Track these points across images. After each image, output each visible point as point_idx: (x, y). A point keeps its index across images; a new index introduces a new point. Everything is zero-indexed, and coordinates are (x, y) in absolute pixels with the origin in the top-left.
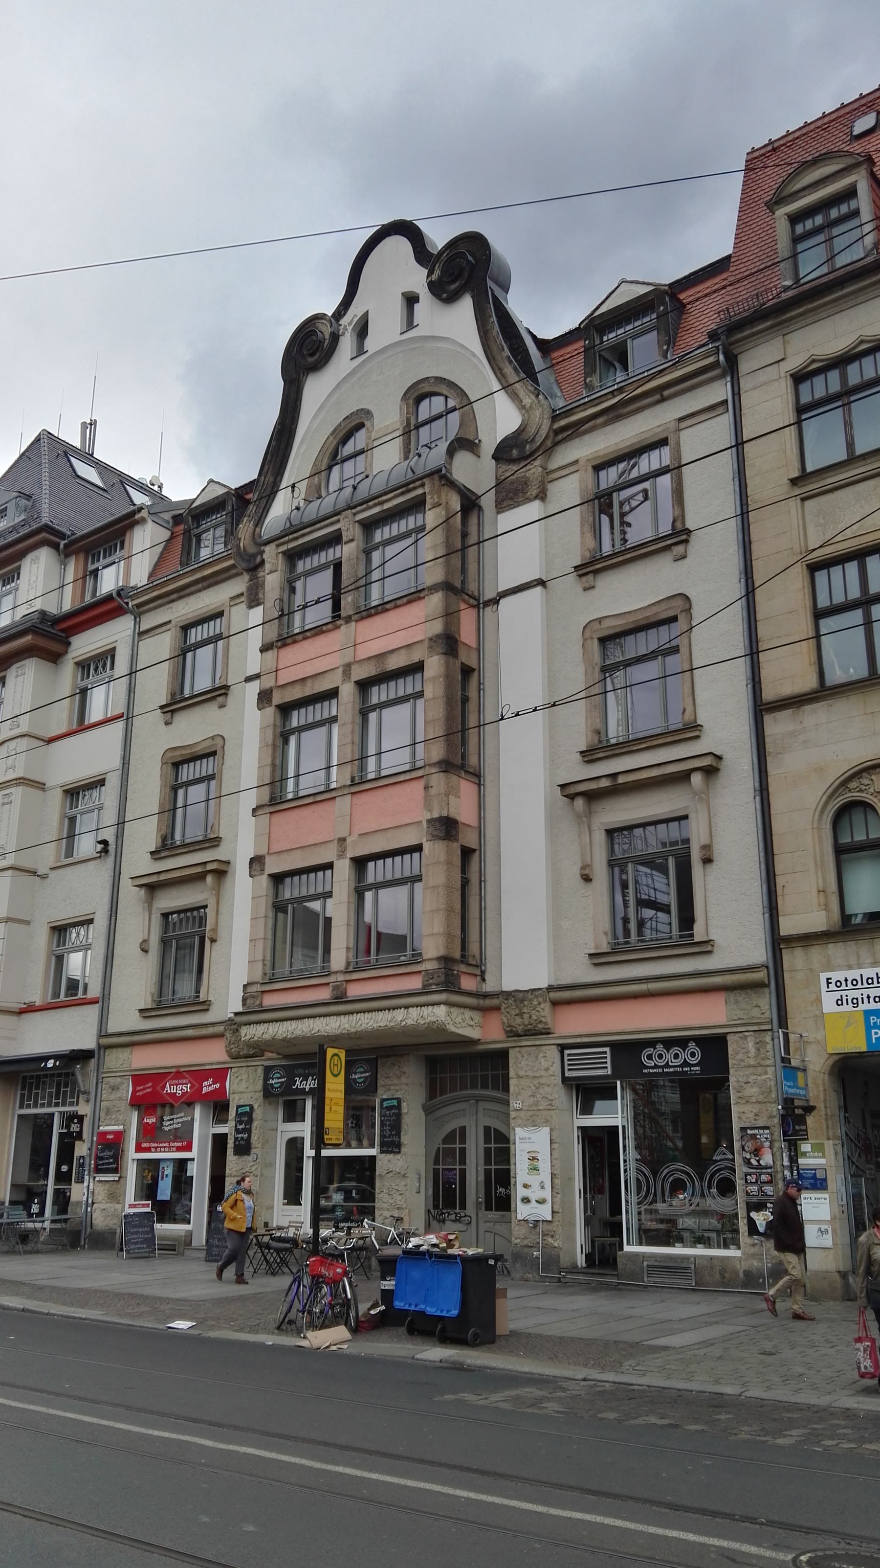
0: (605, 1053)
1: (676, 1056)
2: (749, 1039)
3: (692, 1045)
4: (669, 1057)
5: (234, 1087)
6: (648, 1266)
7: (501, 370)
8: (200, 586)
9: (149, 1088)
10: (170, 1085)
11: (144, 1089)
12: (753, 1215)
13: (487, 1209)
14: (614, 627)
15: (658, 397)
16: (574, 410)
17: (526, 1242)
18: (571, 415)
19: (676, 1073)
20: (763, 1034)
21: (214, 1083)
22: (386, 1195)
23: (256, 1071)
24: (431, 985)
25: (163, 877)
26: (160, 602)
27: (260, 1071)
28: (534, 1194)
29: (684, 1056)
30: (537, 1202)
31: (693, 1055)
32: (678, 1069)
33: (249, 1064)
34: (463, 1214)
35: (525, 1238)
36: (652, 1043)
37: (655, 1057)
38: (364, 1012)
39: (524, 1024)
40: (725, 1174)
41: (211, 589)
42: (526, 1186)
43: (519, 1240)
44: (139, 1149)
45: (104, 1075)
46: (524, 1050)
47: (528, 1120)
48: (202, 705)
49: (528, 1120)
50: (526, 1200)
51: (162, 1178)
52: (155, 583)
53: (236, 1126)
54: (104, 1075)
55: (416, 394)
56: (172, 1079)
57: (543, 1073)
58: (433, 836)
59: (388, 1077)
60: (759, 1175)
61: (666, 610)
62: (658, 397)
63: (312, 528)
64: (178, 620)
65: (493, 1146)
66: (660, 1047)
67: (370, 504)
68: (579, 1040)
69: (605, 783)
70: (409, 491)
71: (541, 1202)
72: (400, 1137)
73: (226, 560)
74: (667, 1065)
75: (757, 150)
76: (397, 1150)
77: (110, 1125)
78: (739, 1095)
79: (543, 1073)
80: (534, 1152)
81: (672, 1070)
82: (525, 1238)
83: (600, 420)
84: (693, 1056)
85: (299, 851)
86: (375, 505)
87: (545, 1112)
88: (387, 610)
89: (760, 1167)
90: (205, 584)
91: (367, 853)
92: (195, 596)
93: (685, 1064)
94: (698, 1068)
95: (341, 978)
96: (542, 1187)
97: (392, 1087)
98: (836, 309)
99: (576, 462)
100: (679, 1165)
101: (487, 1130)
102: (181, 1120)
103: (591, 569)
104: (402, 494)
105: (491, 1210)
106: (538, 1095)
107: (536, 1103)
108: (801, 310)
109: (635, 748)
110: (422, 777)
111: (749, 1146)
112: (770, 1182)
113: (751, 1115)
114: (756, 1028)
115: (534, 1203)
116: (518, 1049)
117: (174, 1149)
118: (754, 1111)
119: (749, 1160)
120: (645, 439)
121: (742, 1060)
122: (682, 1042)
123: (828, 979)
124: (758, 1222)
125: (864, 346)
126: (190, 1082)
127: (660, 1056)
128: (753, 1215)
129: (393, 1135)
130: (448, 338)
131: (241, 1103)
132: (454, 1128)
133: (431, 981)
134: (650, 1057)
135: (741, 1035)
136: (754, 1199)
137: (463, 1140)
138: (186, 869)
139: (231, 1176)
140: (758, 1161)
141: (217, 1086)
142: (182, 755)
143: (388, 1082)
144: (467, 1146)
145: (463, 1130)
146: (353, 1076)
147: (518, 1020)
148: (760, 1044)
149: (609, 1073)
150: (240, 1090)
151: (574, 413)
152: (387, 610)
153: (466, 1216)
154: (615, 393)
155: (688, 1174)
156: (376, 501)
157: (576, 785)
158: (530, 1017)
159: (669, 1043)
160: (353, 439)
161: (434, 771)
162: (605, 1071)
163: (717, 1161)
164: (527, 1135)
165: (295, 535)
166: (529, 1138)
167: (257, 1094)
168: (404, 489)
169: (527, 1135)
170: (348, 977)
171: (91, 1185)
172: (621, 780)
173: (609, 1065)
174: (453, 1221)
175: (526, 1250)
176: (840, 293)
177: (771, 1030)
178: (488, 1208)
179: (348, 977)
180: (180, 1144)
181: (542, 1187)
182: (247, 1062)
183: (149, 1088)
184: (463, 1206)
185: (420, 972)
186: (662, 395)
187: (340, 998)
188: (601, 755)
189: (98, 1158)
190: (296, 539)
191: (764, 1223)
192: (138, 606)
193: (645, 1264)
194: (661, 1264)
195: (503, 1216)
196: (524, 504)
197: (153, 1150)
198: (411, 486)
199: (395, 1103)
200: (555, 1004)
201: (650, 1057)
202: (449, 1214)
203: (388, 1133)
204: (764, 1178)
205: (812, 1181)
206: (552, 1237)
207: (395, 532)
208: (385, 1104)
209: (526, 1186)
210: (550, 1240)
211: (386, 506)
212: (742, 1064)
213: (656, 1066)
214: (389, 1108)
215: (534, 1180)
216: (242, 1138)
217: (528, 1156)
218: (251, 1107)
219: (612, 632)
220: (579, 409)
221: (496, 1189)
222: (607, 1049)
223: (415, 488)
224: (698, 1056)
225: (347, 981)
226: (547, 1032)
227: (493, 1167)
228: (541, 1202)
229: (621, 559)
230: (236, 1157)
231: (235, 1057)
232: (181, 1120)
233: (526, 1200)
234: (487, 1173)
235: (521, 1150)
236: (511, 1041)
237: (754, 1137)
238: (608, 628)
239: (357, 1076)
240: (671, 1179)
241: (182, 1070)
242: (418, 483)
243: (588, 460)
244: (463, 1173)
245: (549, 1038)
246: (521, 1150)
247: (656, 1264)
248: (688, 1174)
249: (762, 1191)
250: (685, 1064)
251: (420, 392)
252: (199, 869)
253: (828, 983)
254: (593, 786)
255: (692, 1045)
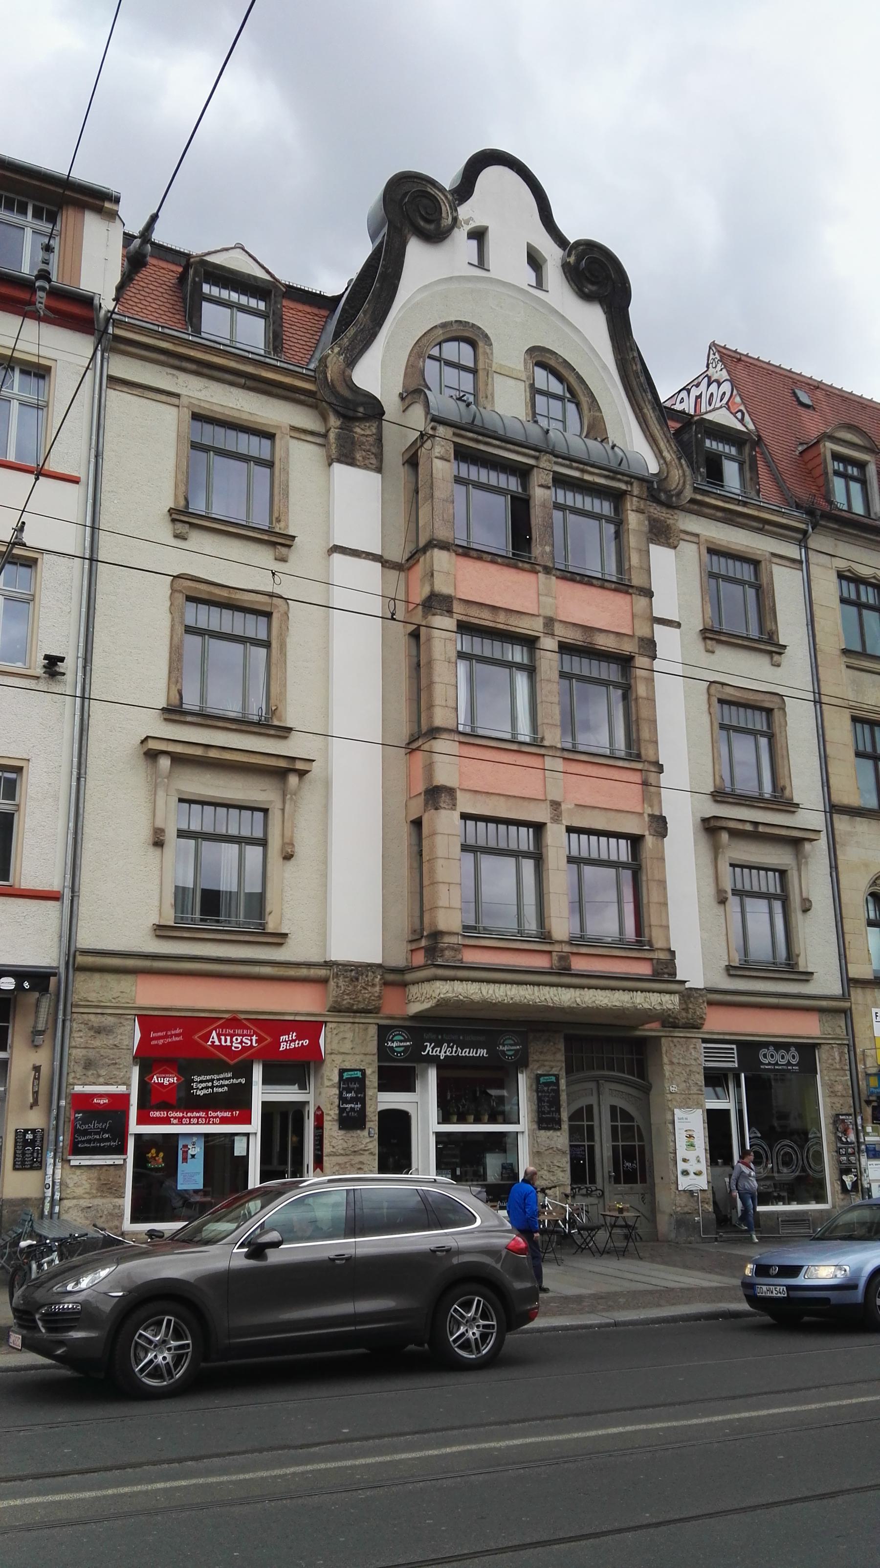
0: (732, 1049)
1: (783, 1057)
2: (835, 1050)
3: (793, 1049)
4: (778, 1057)
5: (335, 1046)
6: (782, 1221)
7: (641, 410)
8: (243, 381)
9: (177, 1035)
10: (219, 1036)
11: (166, 1037)
12: (844, 1177)
13: (615, 1183)
14: (731, 695)
15: (761, 526)
16: (710, 494)
17: (686, 1209)
18: (705, 495)
19: (783, 1070)
20: (843, 1047)
21: (299, 1038)
22: (546, 1173)
23: (366, 1029)
24: (664, 973)
25: (213, 754)
26: (162, 358)
27: (373, 1031)
28: (692, 1167)
29: (788, 1057)
30: (695, 1174)
31: (794, 1057)
32: (785, 1067)
33: (357, 1020)
34: (594, 1188)
35: (686, 1206)
36: (766, 1045)
37: (769, 1057)
38: (596, 989)
39: (687, 1018)
40: (816, 1148)
41: (252, 394)
42: (685, 1160)
43: (679, 1209)
44: (141, 1121)
45: (74, 1010)
46: (675, 1040)
47: (681, 1102)
48: (245, 542)
49: (681, 1102)
50: (685, 1173)
51: (185, 1160)
52: (167, 331)
53: (341, 1094)
54: (74, 1010)
55: (540, 359)
56: (222, 1026)
57: (693, 1062)
58: (656, 831)
59: (541, 1053)
60: (847, 1149)
61: (769, 701)
62: (761, 526)
63: (503, 444)
64: (196, 402)
65: (619, 1124)
66: (771, 1048)
67: (574, 464)
68: (721, 1037)
69: (749, 827)
70: (613, 479)
71: (698, 1174)
72: (560, 1114)
73: (307, 381)
74: (777, 1064)
75: (751, 357)
76: (557, 1127)
77: (94, 1084)
78: (831, 1090)
79: (693, 1062)
80: (690, 1130)
81: (780, 1067)
82: (686, 1206)
83: (719, 514)
84: (793, 1058)
85: (502, 799)
86: (577, 469)
87: (695, 1096)
88: (592, 585)
89: (847, 1143)
90: (249, 383)
91: (612, 830)
92: (222, 386)
93: (789, 1063)
94: (797, 1068)
95: (567, 948)
96: (699, 1161)
97: (547, 1063)
98: (865, 545)
99: (697, 535)
100: (787, 1142)
101: (613, 1109)
102: (227, 1082)
103: (717, 637)
104: (606, 477)
105: (620, 1183)
106: (690, 1081)
107: (689, 1088)
108: (855, 532)
109: (756, 804)
110: (641, 770)
111: (841, 1128)
112: (853, 1154)
113: (839, 1105)
114: (839, 1042)
115: (692, 1175)
116: (670, 1039)
117: (218, 1120)
118: (841, 1102)
119: (841, 1138)
120: (748, 552)
121: (832, 1065)
122: (786, 1046)
123: (876, 1013)
124: (847, 1183)
125: (873, 581)
126: (255, 1033)
127: (783, 1057)
128: (844, 1177)
129: (553, 1112)
130: (580, 331)
131: (347, 1065)
132: (580, 1106)
133: (666, 971)
134: (765, 1056)
135: (830, 1046)
136: (844, 1166)
137: (590, 1117)
138: (258, 756)
139: (334, 1154)
140: (846, 1139)
141: (306, 1042)
142: (210, 593)
143: (542, 1057)
144: (610, 1123)
145: (590, 1108)
146: (501, 1048)
147: (684, 1014)
148: (841, 1054)
149: (737, 1066)
150: (342, 1050)
151: (708, 496)
152: (592, 585)
153: (597, 1190)
154: (741, 503)
155: (791, 1147)
156: (581, 466)
157: (727, 821)
158: (695, 1013)
159: (778, 1046)
160: (210, 259)
161: (653, 769)
162: (733, 1064)
163: (811, 1138)
164: (685, 1116)
165: (480, 438)
166: (686, 1119)
167: (371, 1057)
168: (611, 474)
169: (685, 1116)
170: (575, 950)
171: (58, 1172)
172: (761, 829)
173: (736, 1060)
174: (583, 1195)
175: (688, 1216)
176: (875, 538)
177: (848, 1045)
178: (617, 1181)
179: (575, 950)
180: (227, 1114)
181: (699, 1161)
182: (354, 1017)
183: (177, 1035)
184: (593, 1181)
185: (651, 959)
186: (764, 527)
187: (564, 970)
188: (731, 800)
189: (76, 1131)
190: (477, 441)
191: (850, 1183)
192: (116, 338)
193: (780, 1219)
194: (791, 1219)
195: (631, 1188)
196: (663, 546)
197: (175, 1121)
198: (619, 476)
199: (553, 1079)
200: (711, 1003)
201: (765, 1056)
202: (580, 1189)
203: (547, 1109)
204: (850, 1150)
205: (873, 1153)
206: (707, 1203)
207: (588, 507)
208: (542, 1080)
209: (685, 1160)
210: (706, 1206)
211: (587, 477)
212: (832, 1067)
213: (769, 1064)
214: (547, 1084)
215: (691, 1155)
216: (352, 1109)
217: (685, 1134)
218: (363, 1072)
219: (729, 698)
220: (714, 496)
221: (623, 1164)
222: (734, 1046)
223: (619, 480)
224: (797, 1058)
225: (572, 953)
226: (697, 1027)
227: (620, 1143)
228: (698, 1174)
229: (740, 642)
230: (342, 1132)
231: (336, 1009)
232: (227, 1082)
233: (685, 1173)
234: (615, 1149)
235: (680, 1129)
236: (666, 1031)
237: (843, 1120)
238: (728, 694)
239: (505, 1048)
240: (782, 1153)
241: (243, 1016)
242: (626, 478)
243: (706, 540)
244: (591, 1149)
245: (699, 1033)
246: (680, 1129)
247: (787, 1219)
248: (791, 1147)
249: (849, 1160)
250: (789, 1063)
251: (544, 360)
252: (283, 764)
253: (877, 1016)
254: (740, 826)
255: (793, 1049)
